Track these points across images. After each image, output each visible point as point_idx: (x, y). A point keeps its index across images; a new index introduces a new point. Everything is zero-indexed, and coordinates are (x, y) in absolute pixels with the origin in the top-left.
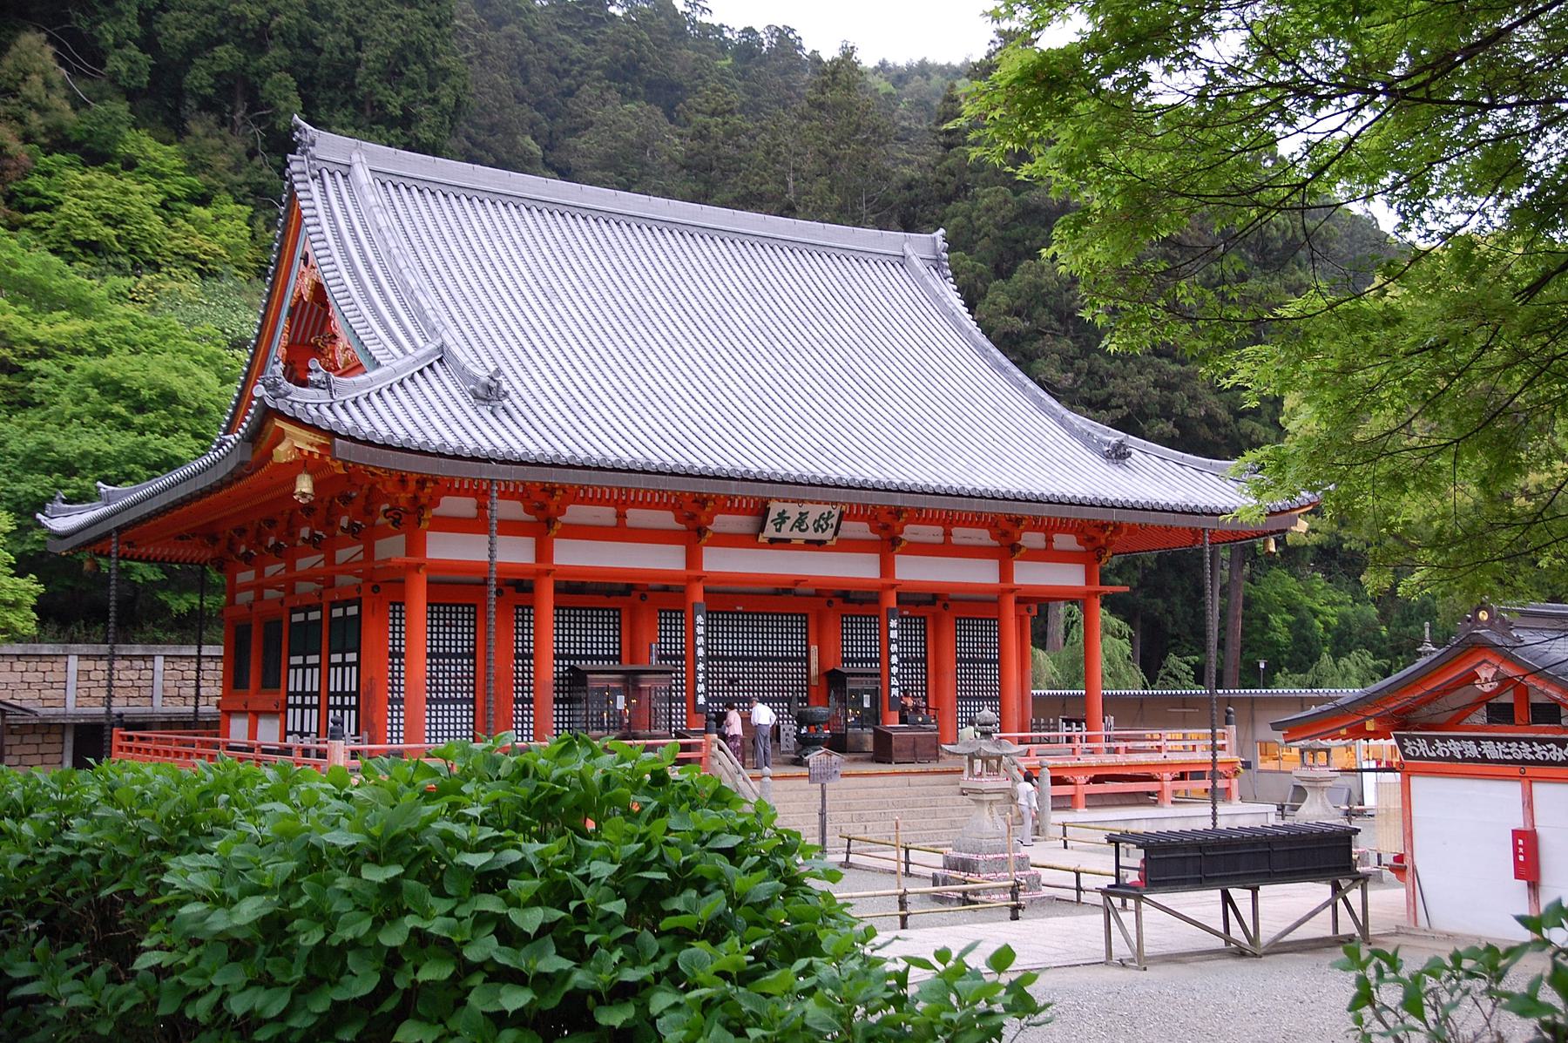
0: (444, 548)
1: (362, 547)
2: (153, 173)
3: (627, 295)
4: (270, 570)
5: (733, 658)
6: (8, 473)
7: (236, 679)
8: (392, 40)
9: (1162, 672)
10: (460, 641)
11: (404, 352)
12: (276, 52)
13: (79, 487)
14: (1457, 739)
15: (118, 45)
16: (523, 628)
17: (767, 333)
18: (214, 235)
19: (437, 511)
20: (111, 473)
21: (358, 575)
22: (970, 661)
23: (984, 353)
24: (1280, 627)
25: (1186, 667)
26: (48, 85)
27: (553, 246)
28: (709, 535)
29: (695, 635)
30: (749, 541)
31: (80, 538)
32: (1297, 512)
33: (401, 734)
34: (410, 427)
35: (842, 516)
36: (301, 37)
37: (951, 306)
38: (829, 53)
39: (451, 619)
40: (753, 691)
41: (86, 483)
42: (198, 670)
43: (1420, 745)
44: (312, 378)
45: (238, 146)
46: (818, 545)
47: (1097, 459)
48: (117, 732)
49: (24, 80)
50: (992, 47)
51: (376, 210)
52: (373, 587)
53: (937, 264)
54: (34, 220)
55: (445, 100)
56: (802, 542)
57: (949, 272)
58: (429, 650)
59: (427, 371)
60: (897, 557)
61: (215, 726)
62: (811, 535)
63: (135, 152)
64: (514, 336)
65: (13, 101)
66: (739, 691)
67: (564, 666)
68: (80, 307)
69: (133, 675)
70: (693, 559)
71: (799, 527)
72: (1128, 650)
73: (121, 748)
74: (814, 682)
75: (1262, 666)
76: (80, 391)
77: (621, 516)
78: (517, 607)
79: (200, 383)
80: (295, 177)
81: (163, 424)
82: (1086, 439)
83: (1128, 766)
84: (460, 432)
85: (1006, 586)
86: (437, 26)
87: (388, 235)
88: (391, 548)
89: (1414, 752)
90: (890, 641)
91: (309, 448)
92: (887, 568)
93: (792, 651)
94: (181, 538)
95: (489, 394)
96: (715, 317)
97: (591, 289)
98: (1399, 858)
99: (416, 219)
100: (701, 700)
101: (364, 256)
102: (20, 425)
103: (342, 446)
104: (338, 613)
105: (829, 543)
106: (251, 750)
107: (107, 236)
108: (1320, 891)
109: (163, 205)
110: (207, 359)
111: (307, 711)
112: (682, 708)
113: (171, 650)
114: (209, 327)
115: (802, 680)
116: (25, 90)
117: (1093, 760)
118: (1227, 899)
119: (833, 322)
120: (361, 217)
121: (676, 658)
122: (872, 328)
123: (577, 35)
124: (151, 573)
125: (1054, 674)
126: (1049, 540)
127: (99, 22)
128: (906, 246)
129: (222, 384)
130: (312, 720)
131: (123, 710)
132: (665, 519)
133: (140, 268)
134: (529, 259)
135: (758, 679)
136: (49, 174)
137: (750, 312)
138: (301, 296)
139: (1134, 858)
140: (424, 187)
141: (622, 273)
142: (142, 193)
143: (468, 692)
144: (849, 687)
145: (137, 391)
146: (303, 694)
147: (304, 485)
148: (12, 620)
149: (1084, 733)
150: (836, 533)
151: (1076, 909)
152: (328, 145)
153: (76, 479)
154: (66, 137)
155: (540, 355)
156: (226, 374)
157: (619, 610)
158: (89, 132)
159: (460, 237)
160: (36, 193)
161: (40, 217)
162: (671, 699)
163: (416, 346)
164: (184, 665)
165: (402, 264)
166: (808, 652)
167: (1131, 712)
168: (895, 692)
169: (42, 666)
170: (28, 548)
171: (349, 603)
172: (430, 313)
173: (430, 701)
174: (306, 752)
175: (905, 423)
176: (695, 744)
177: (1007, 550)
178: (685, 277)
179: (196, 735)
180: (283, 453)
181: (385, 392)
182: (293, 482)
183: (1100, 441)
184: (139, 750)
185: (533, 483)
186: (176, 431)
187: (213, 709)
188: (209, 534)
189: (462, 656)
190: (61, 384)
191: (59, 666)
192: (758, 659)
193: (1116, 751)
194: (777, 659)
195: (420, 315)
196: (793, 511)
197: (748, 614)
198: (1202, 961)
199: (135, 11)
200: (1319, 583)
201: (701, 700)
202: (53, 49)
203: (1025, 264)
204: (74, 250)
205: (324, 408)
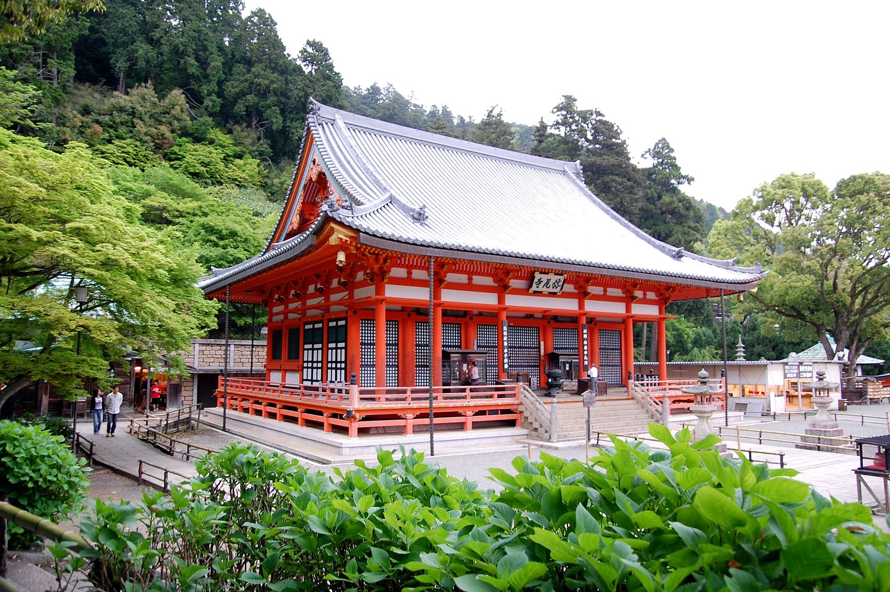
0: (393, 292)
1: (347, 293)
2: (221, 146)
7: (274, 353)
12: (272, 99)
15: (209, 95)
21: (346, 306)
26: (182, 111)
30: (525, 292)
35: (565, 281)
36: (281, 93)
45: (254, 135)
49: (173, 108)
53: (577, 174)
59: (386, 206)
61: (262, 376)
62: (551, 290)
63: (214, 137)
68: (195, 197)
74: (542, 359)
77: (470, 279)
79: (246, 228)
80: (311, 124)
81: (232, 245)
82: (663, 250)
85: (629, 314)
90: (584, 340)
94: (248, 291)
95: (419, 217)
100: (506, 366)
103: (364, 237)
104: (332, 324)
109: (224, 159)
111: (339, 371)
113: (237, 342)
116: (173, 112)
123: (368, 106)
127: (201, 86)
128: (565, 167)
130: (317, 374)
132: (488, 281)
136: (180, 146)
138: (311, 179)
140: (366, 130)
143: (395, 362)
144: (560, 361)
145: (221, 231)
147: (341, 257)
148: (207, 322)
150: (561, 289)
154: (187, 131)
158: (196, 129)
160: (175, 153)
166: (539, 344)
171: (341, 319)
172: (382, 182)
180: (333, 240)
182: (336, 254)
188: (261, 290)
192: (519, 347)
196: (545, 278)
201: (506, 366)
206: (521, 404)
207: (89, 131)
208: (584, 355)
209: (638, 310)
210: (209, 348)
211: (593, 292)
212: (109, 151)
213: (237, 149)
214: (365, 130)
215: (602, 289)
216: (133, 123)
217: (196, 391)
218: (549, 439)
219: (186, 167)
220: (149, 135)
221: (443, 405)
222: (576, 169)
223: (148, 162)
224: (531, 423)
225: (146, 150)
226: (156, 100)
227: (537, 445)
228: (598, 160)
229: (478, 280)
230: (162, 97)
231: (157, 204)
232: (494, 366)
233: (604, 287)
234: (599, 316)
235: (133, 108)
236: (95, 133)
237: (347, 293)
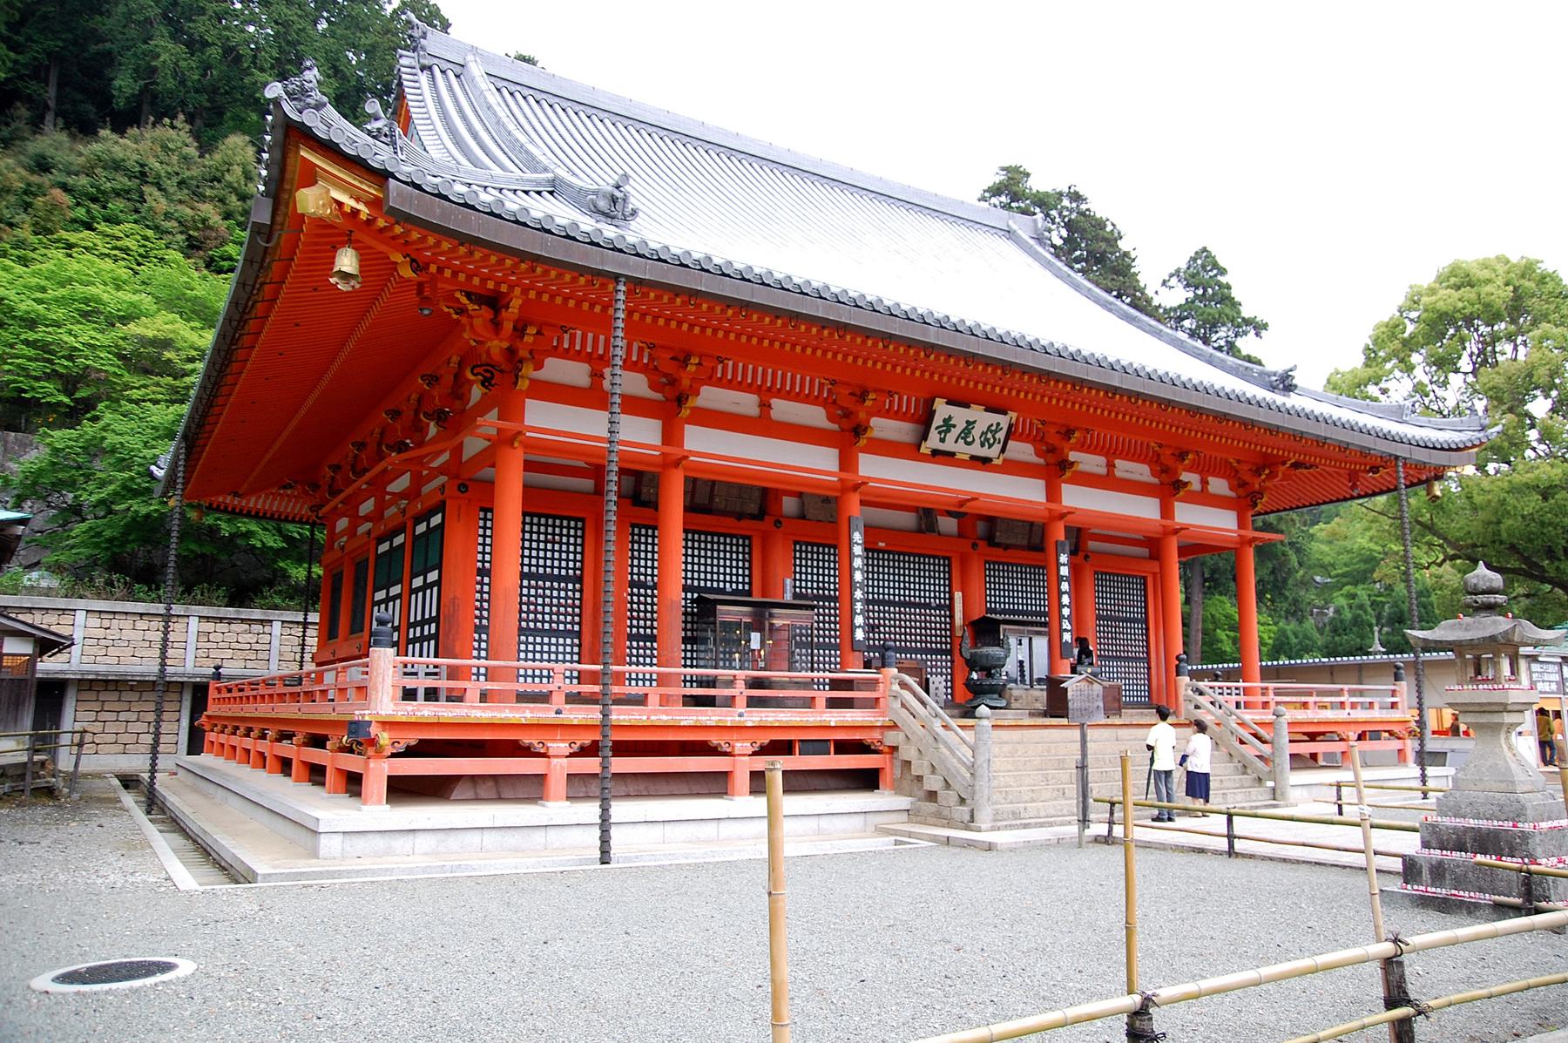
10: (564, 560)
16: (639, 551)
30: (910, 451)
39: (554, 534)
46: (982, 463)
49: (228, 170)
52: (459, 486)
56: (966, 457)
60: (1064, 487)
62: (977, 450)
69: (252, 638)
74: (959, 633)
77: (765, 406)
90: (1060, 579)
100: (859, 635)
105: (995, 462)
115: (946, 630)
116: (228, 177)
126: (765, 406)
128: (1011, 222)
147: (347, 261)
150: (1003, 450)
157: (749, 538)
166: (951, 599)
189: (567, 579)
192: (900, 604)
196: (960, 415)
201: (859, 635)
206: (895, 726)
207: (39, 201)
208: (1061, 617)
209: (1188, 515)
210: (222, 627)
211: (1081, 467)
212: (83, 243)
214: (539, 96)
215: (1102, 460)
216: (142, 195)
218: (970, 823)
221: (664, 719)
224: (920, 778)
226: (192, 151)
227: (934, 839)
229: (1125, 468)
230: (205, 148)
231: (150, 334)
232: (830, 646)
233: (1106, 455)
234: (1097, 526)
235: (142, 166)
236: (55, 206)
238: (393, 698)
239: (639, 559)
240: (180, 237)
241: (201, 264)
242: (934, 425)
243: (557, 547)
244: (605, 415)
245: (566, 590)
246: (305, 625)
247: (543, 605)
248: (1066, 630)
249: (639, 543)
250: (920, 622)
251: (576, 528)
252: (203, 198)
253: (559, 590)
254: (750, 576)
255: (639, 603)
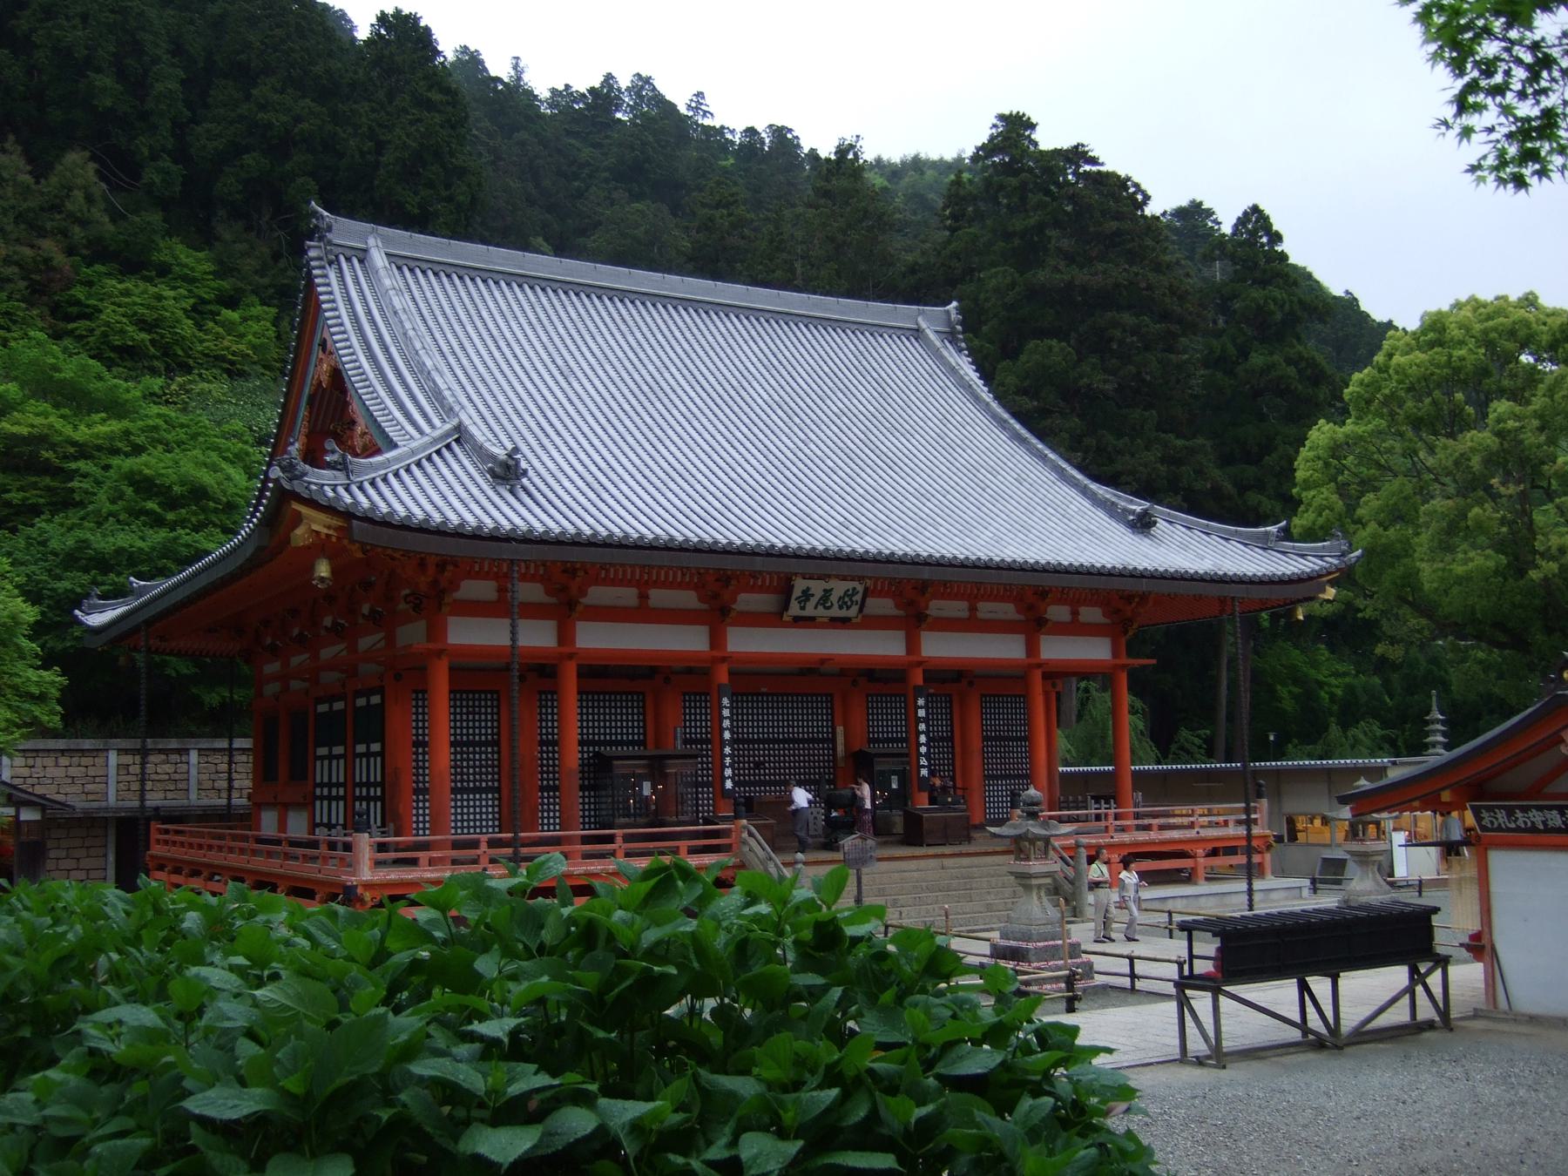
0: (467, 633)
1: (382, 635)
3: (644, 372)
4: (295, 661)
5: (759, 741)
6: (50, 571)
7: (265, 772)
8: (409, 142)
9: (1173, 747)
11: (421, 432)
13: (114, 583)
14: (1539, 808)
15: (154, 157)
16: (547, 714)
17: (785, 407)
18: (242, 336)
19: (459, 595)
20: (145, 569)
22: (996, 739)
23: (1002, 424)
24: (1286, 696)
25: (1197, 741)
26: (90, 199)
27: (569, 325)
28: (733, 614)
29: (721, 718)
30: (773, 619)
31: (114, 633)
32: (1325, 579)
33: (427, 825)
34: (429, 507)
37: (967, 378)
38: (827, 151)
40: (790, 774)
41: (121, 579)
42: (230, 763)
43: (1499, 816)
44: (328, 459)
47: (1122, 528)
48: (155, 826)
49: (68, 196)
50: (994, 131)
51: (392, 293)
53: (951, 337)
54: (77, 329)
55: (461, 198)
56: (826, 620)
57: (963, 345)
58: (452, 738)
59: (445, 452)
61: (247, 819)
62: (836, 612)
64: (532, 415)
65: (58, 217)
66: (765, 775)
67: (588, 752)
68: (116, 408)
69: (168, 768)
70: (717, 640)
71: (823, 605)
72: (1141, 725)
73: (158, 841)
74: (841, 764)
75: (1272, 738)
76: (116, 489)
77: (643, 597)
78: (540, 693)
79: (229, 478)
81: (193, 519)
82: (1110, 509)
83: (1163, 843)
84: (479, 512)
85: (1033, 661)
86: (453, 127)
87: (404, 317)
88: (412, 635)
89: (1492, 823)
90: (918, 720)
91: (325, 531)
92: (913, 645)
93: (818, 732)
95: (507, 473)
96: (733, 393)
97: (608, 367)
98: (1476, 937)
99: (432, 301)
100: (729, 784)
101: (380, 338)
102: (62, 525)
104: (361, 702)
105: (854, 621)
106: (278, 842)
107: (143, 341)
108: (1397, 976)
109: (194, 308)
110: (236, 455)
112: (708, 793)
113: (205, 744)
114: (237, 425)
115: (829, 761)
116: (69, 206)
117: (1126, 838)
118: (1304, 988)
119: (851, 396)
120: (377, 301)
121: (702, 742)
122: (890, 401)
124: (185, 668)
125: (1069, 751)
126: (1075, 613)
129: (250, 479)
130: (338, 812)
131: (159, 803)
132: (687, 599)
133: (173, 370)
134: (545, 339)
135: (785, 762)
136: (90, 284)
137: (767, 387)
138: (320, 383)
139: (1208, 946)
141: (639, 350)
142: (175, 299)
144: (877, 768)
145: (170, 487)
146: (330, 785)
147: (323, 570)
148: (37, 713)
149: (1113, 811)
150: (861, 610)
151: (1131, 998)
152: (345, 230)
153: (112, 575)
155: (559, 434)
156: (254, 470)
159: (476, 319)
160: (78, 303)
161: (80, 326)
162: (697, 785)
163: (433, 426)
164: (217, 758)
165: (418, 345)
166: (834, 733)
167: (1161, 789)
168: (924, 772)
169: (85, 761)
170: (68, 644)
172: (447, 393)
173: (454, 791)
174: (332, 846)
175: (928, 496)
176: (723, 830)
177: (1033, 626)
178: (701, 353)
179: (230, 828)
180: (300, 535)
181: (402, 473)
182: (311, 568)
183: (1125, 510)
184: (174, 843)
185: (554, 562)
186: (206, 526)
187: (244, 801)
189: (486, 744)
190: (98, 483)
191: (100, 761)
192: (784, 741)
193: (1148, 828)
194: (803, 741)
195: (436, 396)
196: (817, 587)
197: (773, 695)
198: (1281, 1055)
199: (169, 125)
200: (1323, 655)
201: (729, 784)
202: (96, 166)
203: (1031, 344)
204: (112, 355)
205: (341, 490)
209: (1056, 650)
213: (225, 284)
217: (111, 858)
219: (104, 334)
220: (17, 264)
222: (949, 323)
223: (14, 328)
225: (10, 298)
226: (26, 178)
228: (1081, 276)
230: (40, 169)
231: (25, 431)
237: (382, 635)
238: (370, 869)
239: (547, 721)
240: (22, 284)
241: (46, 310)
242: (794, 597)
243: (477, 717)
244: (507, 622)
245: (486, 753)
246: (230, 751)
247: (468, 767)
248: (924, 766)
249: (546, 707)
250: (804, 756)
251: (492, 700)
252: (43, 233)
253: (480, 753)
254: (644, 727)
255: (548, 759)
